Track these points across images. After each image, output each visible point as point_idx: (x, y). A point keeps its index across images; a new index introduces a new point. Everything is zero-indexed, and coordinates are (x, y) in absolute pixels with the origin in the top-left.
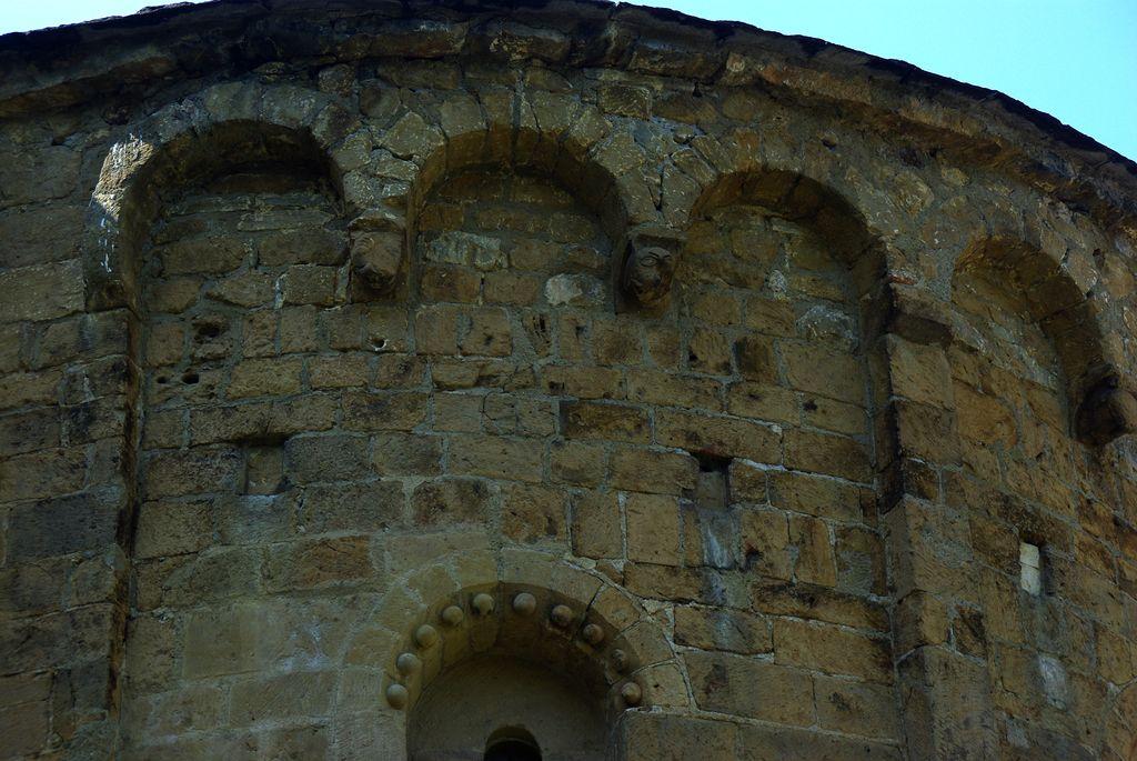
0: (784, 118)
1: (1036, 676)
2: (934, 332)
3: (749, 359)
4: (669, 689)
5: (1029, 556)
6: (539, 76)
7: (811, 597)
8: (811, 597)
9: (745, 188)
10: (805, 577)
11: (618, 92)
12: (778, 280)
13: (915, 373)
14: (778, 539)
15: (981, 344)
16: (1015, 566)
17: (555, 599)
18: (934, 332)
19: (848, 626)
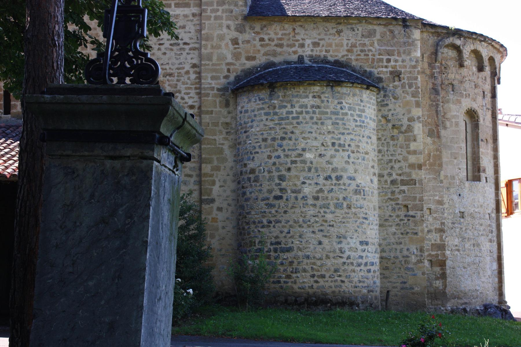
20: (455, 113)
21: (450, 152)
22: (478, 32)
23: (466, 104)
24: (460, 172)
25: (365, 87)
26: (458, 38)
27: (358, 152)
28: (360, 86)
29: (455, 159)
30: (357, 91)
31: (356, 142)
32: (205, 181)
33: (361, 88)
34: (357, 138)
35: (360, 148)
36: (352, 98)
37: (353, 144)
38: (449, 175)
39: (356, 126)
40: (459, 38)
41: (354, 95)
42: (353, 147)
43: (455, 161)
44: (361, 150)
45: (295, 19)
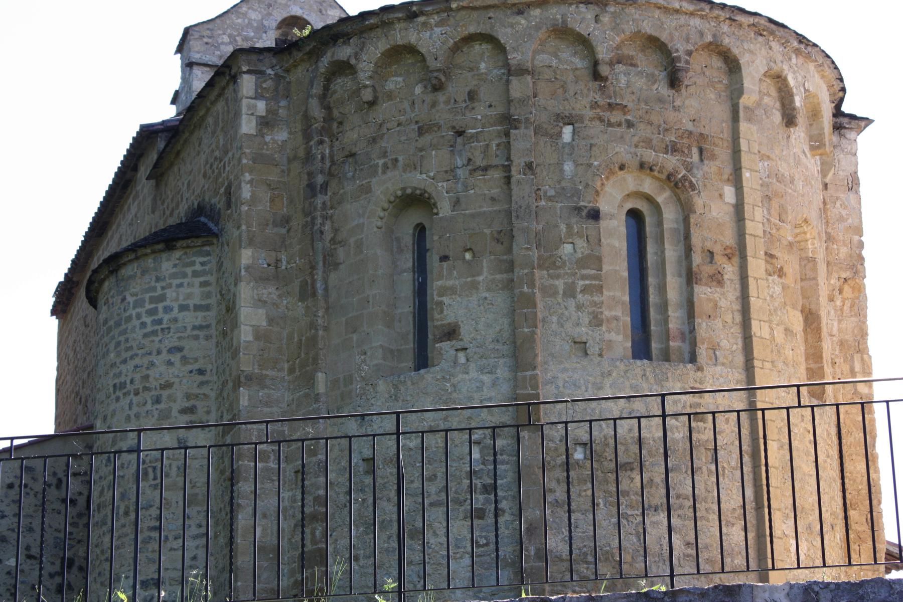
0: (475, 14)
1: (562, 171)
2: (522, 71)
3: (472, 96)
4: (445, 209)
5: (567, 131)
6: (403, 25)
7: (485, 169)
8: (485, 169)
9: (470, 39)
10: (484, 163)
11: (424, 24)
12: (483, 66)
13: (518, 88)
14: (477, 153)
15: (554, 63)
16: (560, 134)
17: (416, 189)
18: (522, 71)
19: (496, 175)
20: (356, 222)
21: (344, 319)
22: (375, 6)
23: (386, 186)
24: (364, 361)
25: (161, 246)
26: (344, 43)
27: (146, 389)
28: (149, 251)
29: (354, 332)
30: (150, 262)
31: (144, 369)
32: (511, 455)
33: (154, 252)
34: (146, 361)
35: (151, 379)
36: (139, 281)
37: (137, 377)
38: (341, 376)
39: (145, 336)
40: (346, 43)
41: (144, 272)
42: (138, 385)
43: (355, 337)
44: (153, 383)
45: (508, 82)
